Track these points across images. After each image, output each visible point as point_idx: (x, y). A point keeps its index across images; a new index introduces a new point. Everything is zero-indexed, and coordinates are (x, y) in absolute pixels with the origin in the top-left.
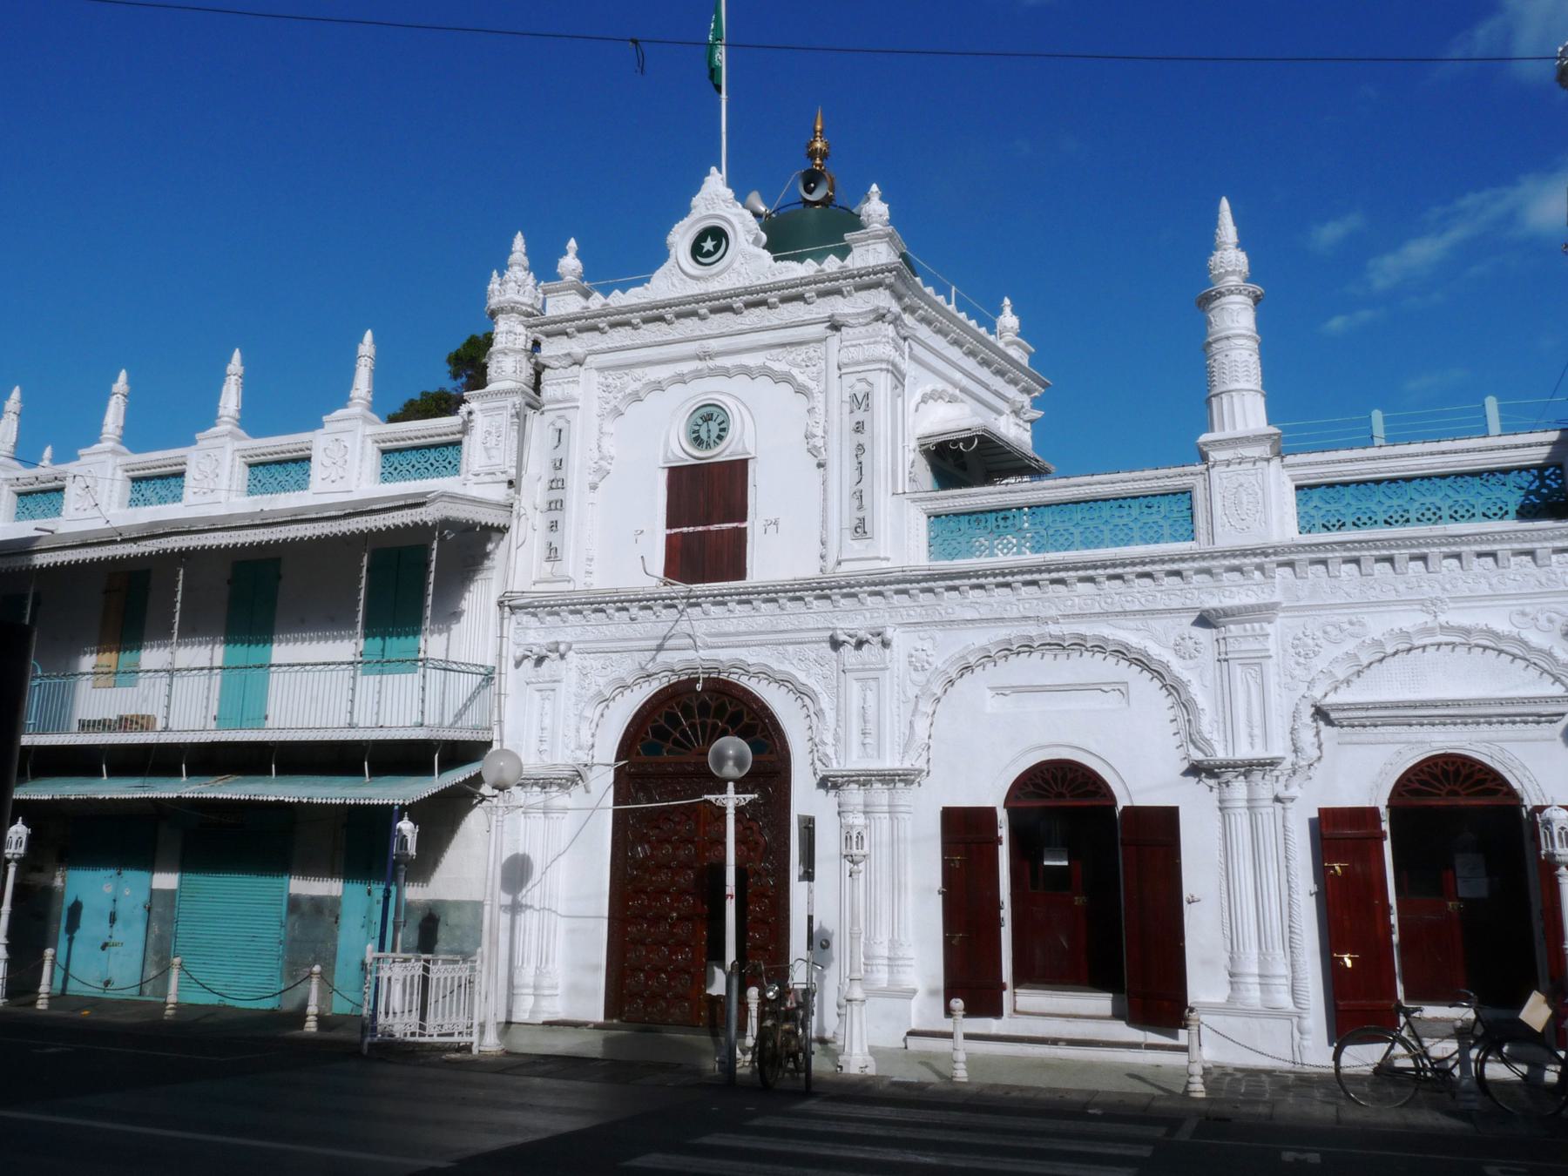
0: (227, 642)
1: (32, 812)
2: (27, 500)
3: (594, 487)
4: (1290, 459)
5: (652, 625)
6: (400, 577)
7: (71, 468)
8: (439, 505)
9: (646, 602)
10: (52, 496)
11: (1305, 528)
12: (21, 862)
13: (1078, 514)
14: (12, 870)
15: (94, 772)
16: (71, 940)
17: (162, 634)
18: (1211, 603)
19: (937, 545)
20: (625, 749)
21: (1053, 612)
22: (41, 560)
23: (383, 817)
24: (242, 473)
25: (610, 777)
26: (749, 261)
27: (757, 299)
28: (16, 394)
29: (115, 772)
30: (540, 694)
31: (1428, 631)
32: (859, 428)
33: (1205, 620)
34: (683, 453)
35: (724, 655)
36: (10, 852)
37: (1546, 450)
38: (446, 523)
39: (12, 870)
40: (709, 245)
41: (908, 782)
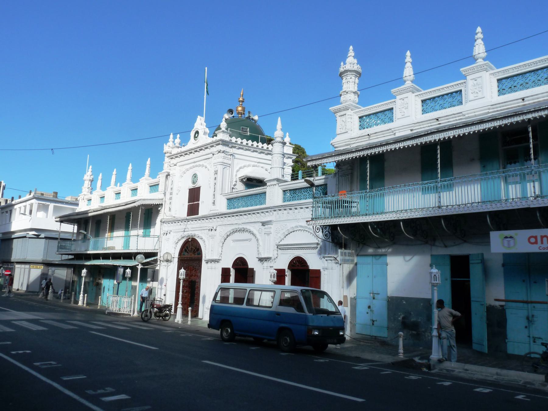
0: (144, 229)
1: (87, 267)
2: (152, 188)
3: (177, 194)
4: (280, 185)
5: (183, 226)
6: (148, 214)
7: (105, 192)
8: (139, 202)
9: (183, 220)
10: (157, 186)
11: (284, 201)
12: (85, 277)
13: (249, 198)
14: (83, 279)
15: (109, 259)
16: (203, 306)
17: (135, 226)
18: (264, 220)
19: (229, 207)
20: (181, 253)
21: (240, 223)
22: (90, 215)
23: (116, 268)
24: (148, 188)
25: (177, 259)
26: (204, 139)
27: (205, 147)
28: (101, 175)
29: (103, 259)
30: (163, 241)
31: (297, 227)
32: (215, 179)
33: (264, 224)
34: (191, 186)
35: (193, 233)
36: (82, 275)
37: (323, 180)
38: (143, 205)
39: (83, 279)
40: (197, 135)
41: (218, 262)
